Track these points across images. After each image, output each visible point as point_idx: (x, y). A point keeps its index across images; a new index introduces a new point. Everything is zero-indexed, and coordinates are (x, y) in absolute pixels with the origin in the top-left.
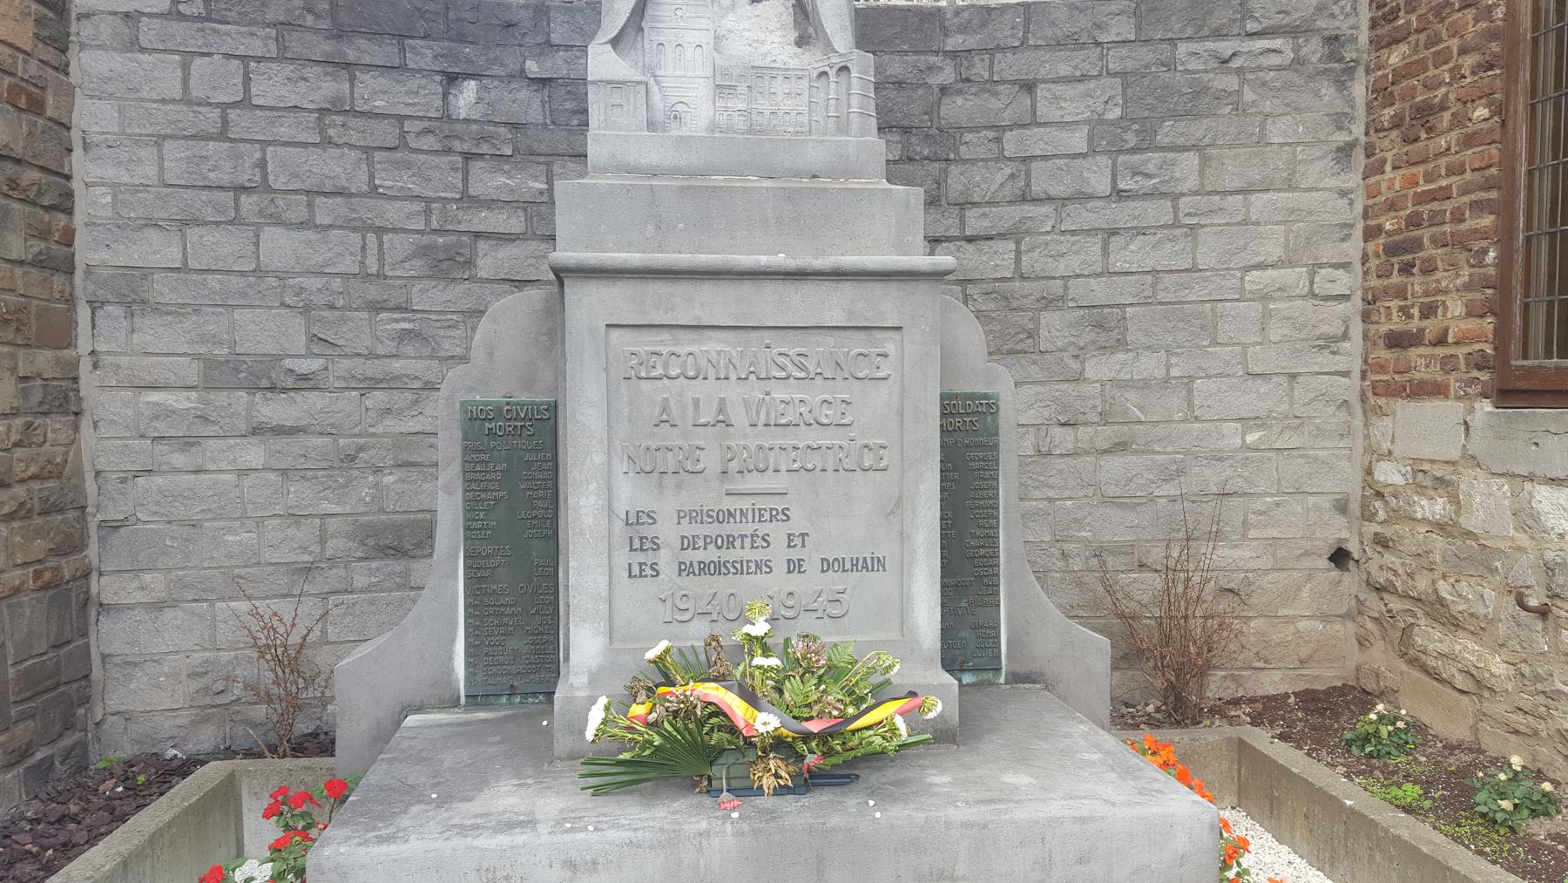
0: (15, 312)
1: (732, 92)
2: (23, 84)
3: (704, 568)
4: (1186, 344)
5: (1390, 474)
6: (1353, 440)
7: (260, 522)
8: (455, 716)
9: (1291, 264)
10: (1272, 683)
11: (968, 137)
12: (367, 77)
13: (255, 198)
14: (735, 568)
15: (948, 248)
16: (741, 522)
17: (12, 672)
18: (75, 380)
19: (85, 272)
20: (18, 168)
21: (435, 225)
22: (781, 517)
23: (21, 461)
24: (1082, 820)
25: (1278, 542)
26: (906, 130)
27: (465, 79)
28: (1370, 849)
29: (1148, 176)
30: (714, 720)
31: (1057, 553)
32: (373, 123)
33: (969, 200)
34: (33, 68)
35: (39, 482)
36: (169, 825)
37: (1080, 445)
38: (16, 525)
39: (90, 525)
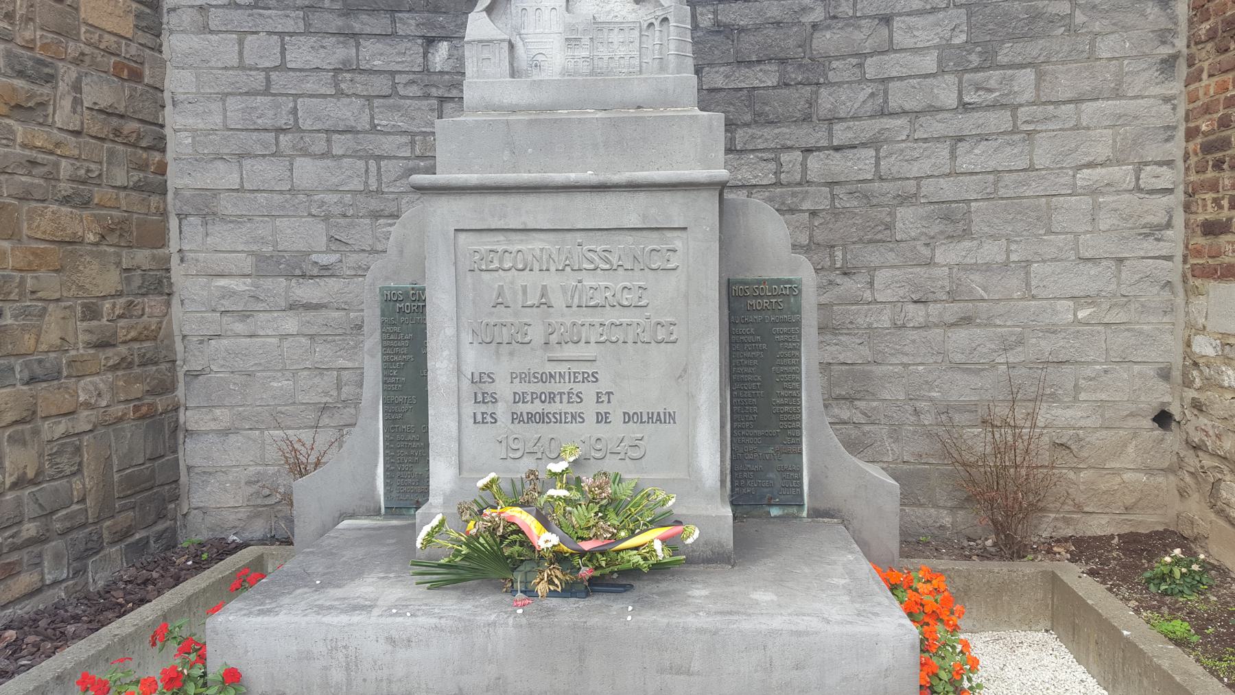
0: (119, 223)
1: (578, 43)
2: (126, 61)
3: (531, 418)
4: (1024, 233)
5: (1204, 347)
6: (1176, 316)
7: (295, 373)
8: (378, 522)
9: (1119, 163)
10: (1098, 526)
11: (835, 64)
12: (368, 43)
13: (290, 136)
14: (556, 418)
15: (818, 156)
16: (560, 382)
17: (116, 477)
18: (168, 270)
19: (174, 194)
20: (122, 121)
21: (418, 152)
22: (591, 379)
23: (123, 328)
24: (799, 634)
25: (1106, 404)
26: (783, 61)
27: (440, 41)
28: (1140, 674)
29: (990, 90)
30: (515, 536)
31: (909, 409)
32: (374, 78)
33: (836, 116)
34: (133, 49)
35: (138, 343)
36: (204, 590)
37: (930, 319)
38: (120, 373)
39: (178, 374)
